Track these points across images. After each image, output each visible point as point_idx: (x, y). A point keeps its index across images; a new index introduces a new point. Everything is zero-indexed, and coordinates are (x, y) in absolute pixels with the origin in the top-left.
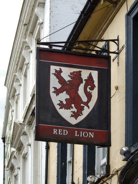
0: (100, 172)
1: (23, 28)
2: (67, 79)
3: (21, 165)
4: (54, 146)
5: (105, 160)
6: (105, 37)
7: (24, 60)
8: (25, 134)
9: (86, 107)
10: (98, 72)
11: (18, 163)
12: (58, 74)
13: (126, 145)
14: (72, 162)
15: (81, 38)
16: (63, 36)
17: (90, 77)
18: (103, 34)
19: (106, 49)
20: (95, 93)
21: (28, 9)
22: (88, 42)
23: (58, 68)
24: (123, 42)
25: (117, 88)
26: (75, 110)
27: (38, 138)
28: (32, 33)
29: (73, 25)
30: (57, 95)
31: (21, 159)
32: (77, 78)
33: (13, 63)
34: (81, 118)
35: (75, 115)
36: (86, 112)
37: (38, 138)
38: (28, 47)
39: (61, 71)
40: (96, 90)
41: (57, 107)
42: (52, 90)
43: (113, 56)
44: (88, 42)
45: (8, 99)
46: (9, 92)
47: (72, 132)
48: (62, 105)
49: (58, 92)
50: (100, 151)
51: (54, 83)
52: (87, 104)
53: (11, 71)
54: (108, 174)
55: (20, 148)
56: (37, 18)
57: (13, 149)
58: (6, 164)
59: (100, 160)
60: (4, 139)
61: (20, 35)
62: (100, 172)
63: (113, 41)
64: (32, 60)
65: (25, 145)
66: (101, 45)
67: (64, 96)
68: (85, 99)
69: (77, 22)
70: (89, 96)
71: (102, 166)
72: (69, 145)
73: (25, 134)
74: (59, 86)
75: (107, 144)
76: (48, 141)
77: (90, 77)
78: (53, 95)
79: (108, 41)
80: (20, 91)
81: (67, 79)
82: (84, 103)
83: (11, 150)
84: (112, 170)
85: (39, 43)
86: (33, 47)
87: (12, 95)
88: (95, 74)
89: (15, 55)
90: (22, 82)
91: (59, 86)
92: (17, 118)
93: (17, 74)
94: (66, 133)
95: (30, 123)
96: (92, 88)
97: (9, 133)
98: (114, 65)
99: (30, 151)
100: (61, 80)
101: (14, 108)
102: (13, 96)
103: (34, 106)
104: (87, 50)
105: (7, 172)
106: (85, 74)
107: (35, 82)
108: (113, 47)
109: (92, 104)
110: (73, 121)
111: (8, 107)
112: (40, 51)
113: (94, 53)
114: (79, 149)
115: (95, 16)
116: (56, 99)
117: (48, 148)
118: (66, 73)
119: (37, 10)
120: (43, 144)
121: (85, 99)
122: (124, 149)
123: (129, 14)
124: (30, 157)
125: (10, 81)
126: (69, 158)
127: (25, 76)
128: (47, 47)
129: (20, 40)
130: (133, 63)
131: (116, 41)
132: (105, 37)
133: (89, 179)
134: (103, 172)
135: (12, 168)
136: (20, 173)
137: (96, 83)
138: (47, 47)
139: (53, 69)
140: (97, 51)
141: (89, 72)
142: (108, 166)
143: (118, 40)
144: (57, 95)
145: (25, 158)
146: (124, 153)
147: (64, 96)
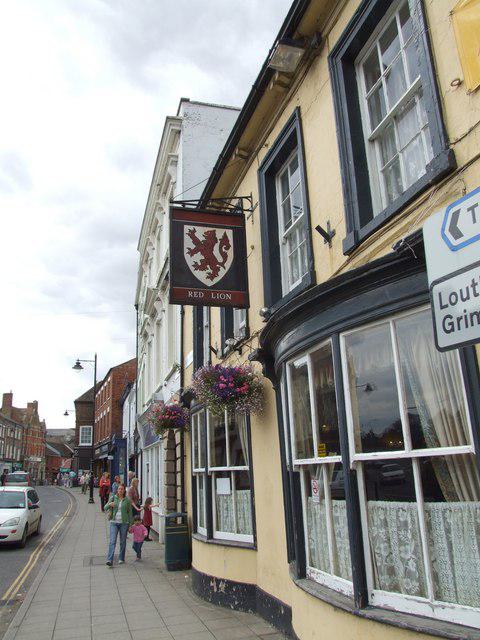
0: (238, 335)
1: (156, 188)
2: (201, 238)
3: (154, 332)
4: (189, 309)
5: (244, 323)
6: (238, 194)
7: (157, 222)
8: (159, 299)
9: (221, 268)
10: (221, 310)
11: (152, 330)
12: (192, 234)
13: (265, 306)
14: (209, 326)
15: (214, 195)
16: (196, 194)
17: (225, 236)
18: (235, 192)
19: (240, 207)
20: (230, 253)
21: (161, 169)
22: (221, 200)
23: (191, 228)
24: (256, 199)
25: (253, 248)
26: (210, 271)
27: (172, 301)
28: (165, 193)
29: (206, 182)
30: (192, 255)
31: (155, 326)
32: (211, 237)
33: (147, 225)
34: (217, 280)
35: (211, 277)
36: (222, 273)
37: (172, 301)
38: (151, 244)
39: (195, 231)
40: (231, 250)
41: (192, 269)
42: (186, 251)
43: (247, 214)
44: (221, 200)
45: (141, 264)
46: (142, 257)
47: (208, 294)
48: (196, 267)
49: (192, 253)
50: (238, 313)
51: (188, 243)
52: (222, 264)
53: (144, 235)
54: (248, 337)
55: (153, 315)
56: (170, 178)
57: (146, 316)
58: (140, 331)
59: (239, 323)
60: (137, 306)
61: (154, 196)
62: (238, 335)
63: (246, 198)
64: (165, 222)
65: (150, 334)
66: (235, 202)
67: (199, 257)
68: (220, 259)
69: (210, 179)
70: (225, 256)
71: (241, 330)
72: (205, 308)
73: (159, 299)
74: (193, 247)
75: (245, 304)
76: (183, 303)
77: (225, 236)
78: (187, 256)
79: (241, 198)
80: (153, 255)
81: (201, 238)
82: (219, 264)
83: (144, 316)
84: (252, 332)
85: (172, 202)
86: (167, 209)
87: (146, 259)
88: (230, 233)
89: (149, 217)
90: (155, 245)
91: (193, 247)
92: (150, 283)
93: (160, 201)
94: (201, 295)
95: (164, 288)
96: (228, 248)
97: (142, 300)
98: (248, 223)
99: (164, 317)
100: (195, 241)
101: (147, 273)
102: (147, 261)
103: (168, 270)
104: (220, 208)
105: (141, 340)
106: (220, 233)
107: (168, 245)
108: (247, 205)
109: (228, 264)
110: (209, 283)
111: (141, 272)
112: (173, 211)
113: (228, 211)
114: (216, 312)
115: (227, 172)
116: (191, 260)
117: (183, 313)
118: (201, 232)
119: (169, 169)
120: (178, 308)
121: (220, 259)
122: (264, 310)
123: (260, 170)
124: (165, 323)
125: (143, 245)
126: (205, 323)
127: (159, 239)
128: (180, 205)
129: (154, 200)
130: (269, 221)
131: (249, 198)
132: (238, 194)
133: (227, 342)
134: (242, 335)
135: (146, 335)
136: (154, 340)
137: (231, 243)
138: (180, 205)
139: (187, 228)
140: (231, 209)
141: (223, 231)
142: (247, 329)
143: (251, 197)
144: (192, 255)
145: (159, 324)
146: (264, 315)
147: (199, 257)
